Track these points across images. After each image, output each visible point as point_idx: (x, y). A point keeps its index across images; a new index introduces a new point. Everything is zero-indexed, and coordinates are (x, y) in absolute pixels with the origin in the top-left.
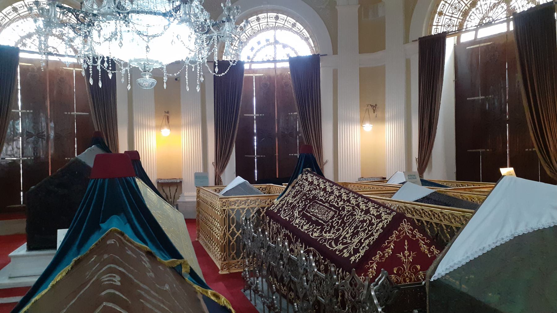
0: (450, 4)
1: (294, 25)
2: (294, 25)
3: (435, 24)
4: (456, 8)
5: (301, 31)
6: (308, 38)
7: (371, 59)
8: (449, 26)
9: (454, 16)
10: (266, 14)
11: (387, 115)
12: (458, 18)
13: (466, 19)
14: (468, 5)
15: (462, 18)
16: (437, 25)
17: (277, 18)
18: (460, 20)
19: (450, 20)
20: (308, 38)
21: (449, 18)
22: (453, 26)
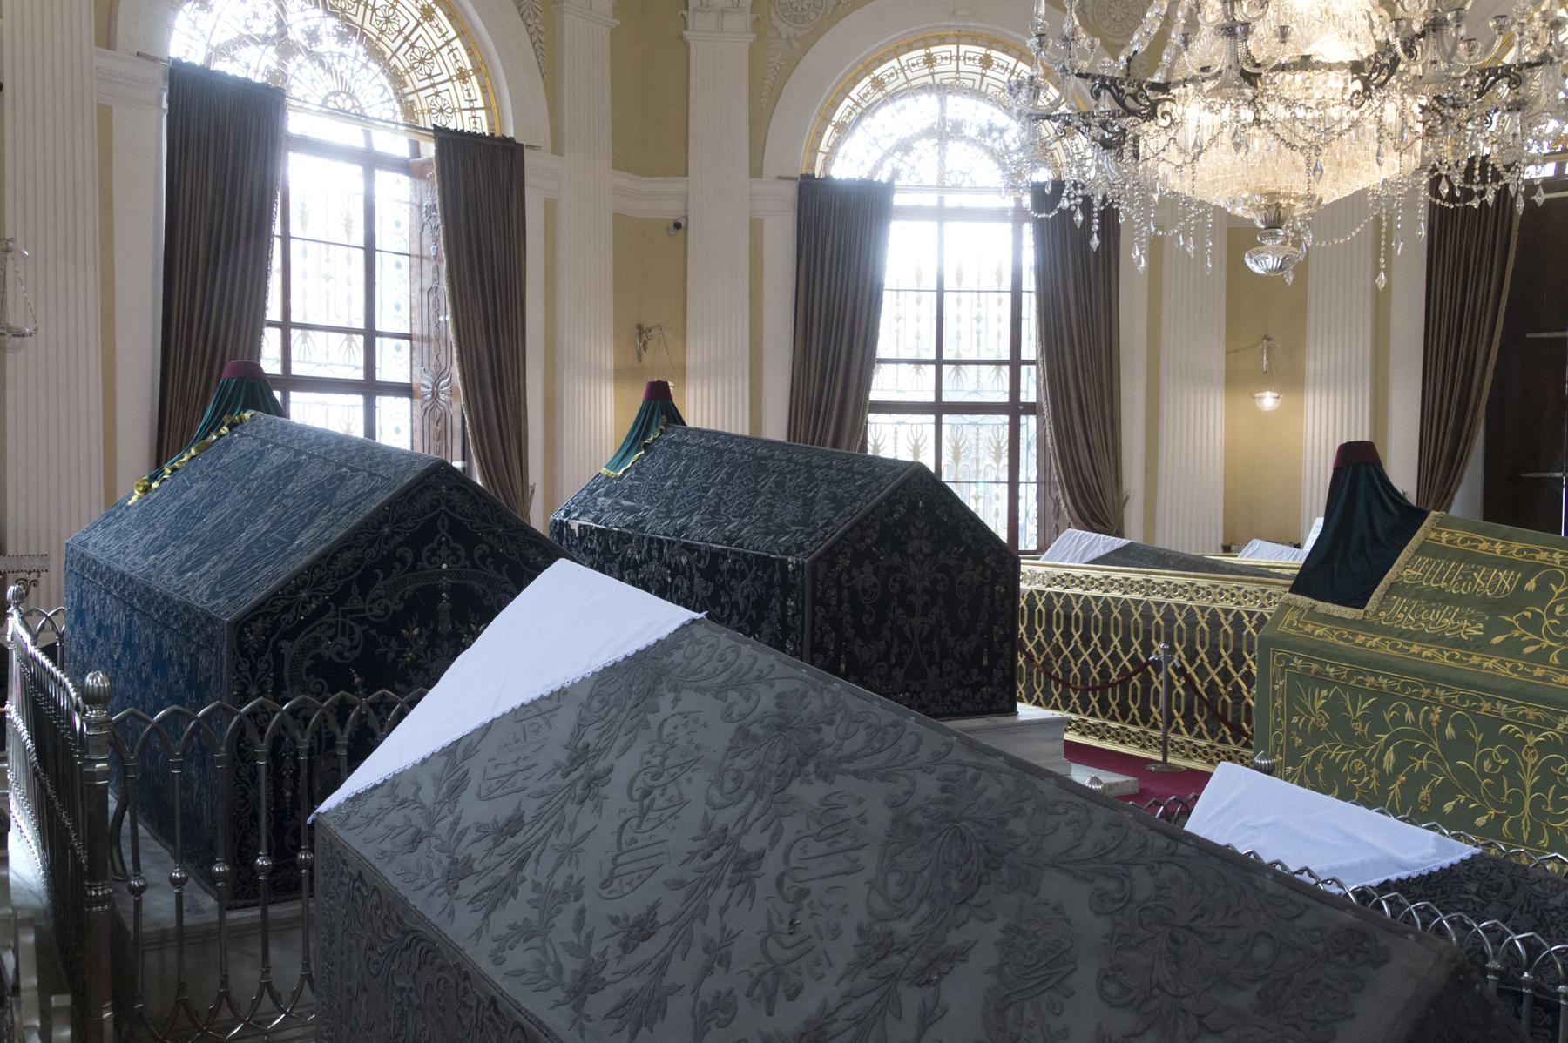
0: (438, 50)
1: (878, 84)
2: (878, 84)
3: (457, 43)
4: (422, 61)
5: (857, 104)
6: (837, 126)
7: (657, 198)
8: (388, 20)
9: (406, 46)
10: (953, 48)
11: (1311, 367)
12: (394, 54)
13: (400, 101)
14: (394, 61)
15: (410, 98)
16: (448, 43)
17: (930, 60)
18: (407, 90)
19: (430, 77)
20: (837, 126)
21: (437, 80)
22: (382, 32)
